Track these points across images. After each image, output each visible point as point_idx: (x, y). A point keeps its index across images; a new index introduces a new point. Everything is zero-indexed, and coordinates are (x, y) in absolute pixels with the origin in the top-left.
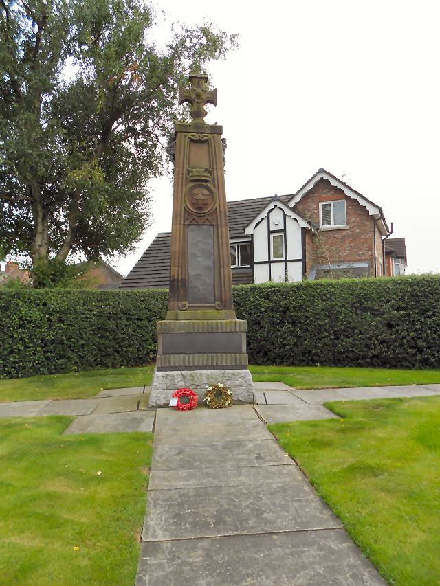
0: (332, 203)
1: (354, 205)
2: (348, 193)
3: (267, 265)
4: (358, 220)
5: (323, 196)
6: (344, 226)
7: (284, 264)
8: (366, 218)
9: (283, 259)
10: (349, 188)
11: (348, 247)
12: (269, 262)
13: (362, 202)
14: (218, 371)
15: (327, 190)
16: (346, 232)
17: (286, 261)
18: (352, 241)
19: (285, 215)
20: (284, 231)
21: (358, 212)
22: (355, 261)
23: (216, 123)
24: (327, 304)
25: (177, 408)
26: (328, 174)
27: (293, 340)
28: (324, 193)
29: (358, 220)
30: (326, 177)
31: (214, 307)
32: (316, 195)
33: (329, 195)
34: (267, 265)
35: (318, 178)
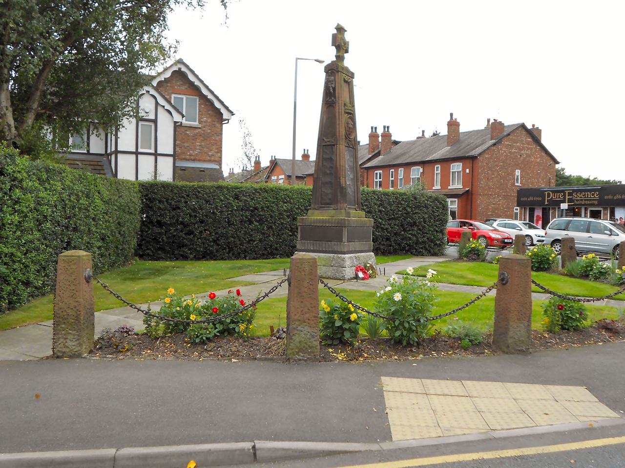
0: (184, 97)
1: (207, 105)
2: (205, 91)
3: (159, 158)
4: (209, 120)
5: (176, 87)
6: (196, 124)
7: (159, 158)
8: (217, 120)
9: (152, 151)
10: (207, 87)
11: (200, 146)
12: (137, 153)
13: (217, 105)
14: (332, 255)
15: (181, 83)
16: (197, 131)
17: (156, 155)
18: (202, 141)
19: (157, 104)
20: (155, 121)
21: (209, 112)
22: (205, 161)
23: (489, 121)
24: (289, 206)
25: (363, 279)
26: (187, 66)
27: (259, 236)
28: (178, 84)
29: (209, 120)
30: (184, 69)
31: (355, 208)
32: (169, 85)
33: (183, 88)
34: (153, 158)
35: (175, 68)
